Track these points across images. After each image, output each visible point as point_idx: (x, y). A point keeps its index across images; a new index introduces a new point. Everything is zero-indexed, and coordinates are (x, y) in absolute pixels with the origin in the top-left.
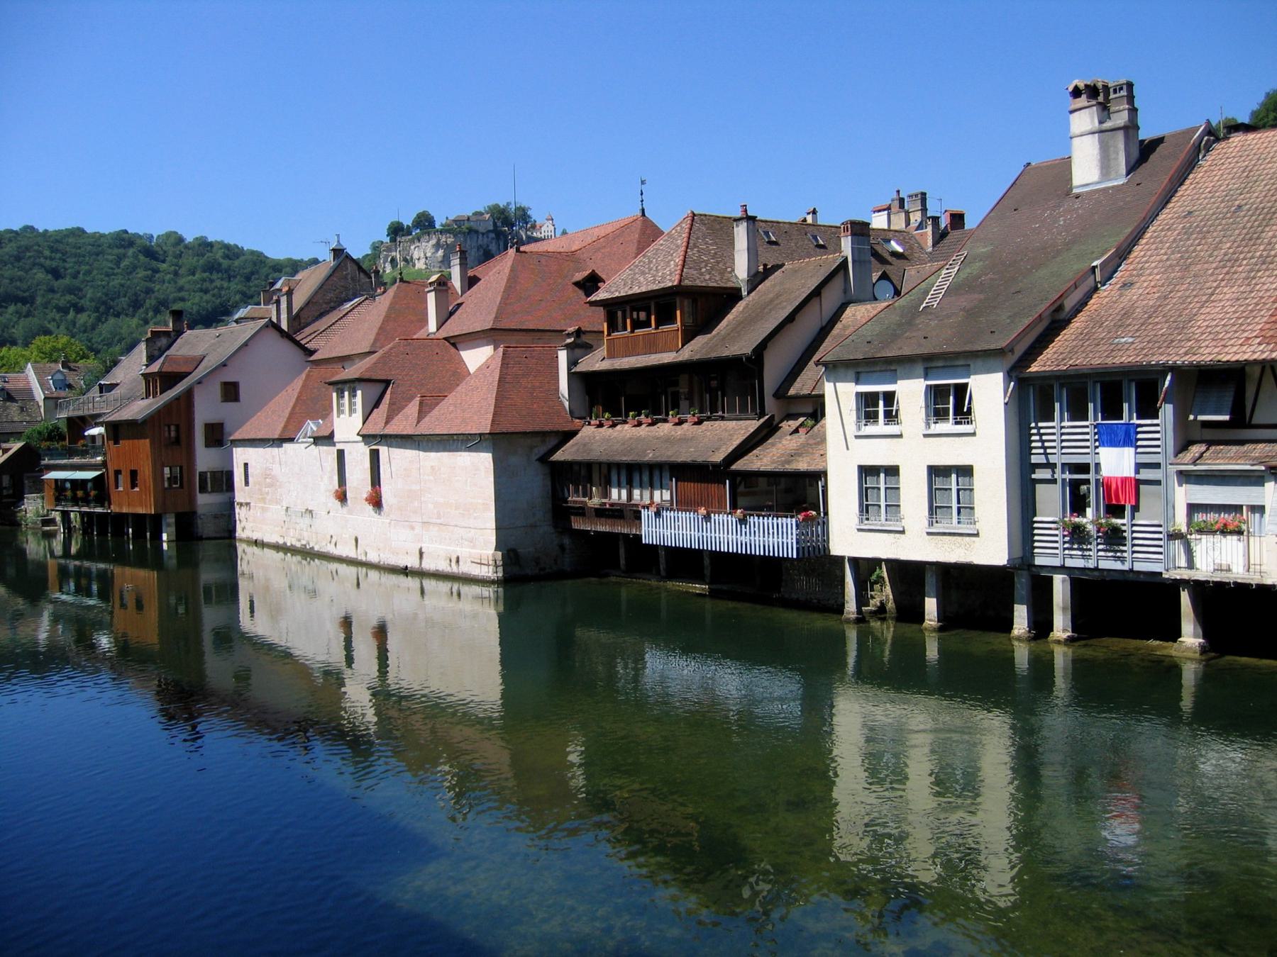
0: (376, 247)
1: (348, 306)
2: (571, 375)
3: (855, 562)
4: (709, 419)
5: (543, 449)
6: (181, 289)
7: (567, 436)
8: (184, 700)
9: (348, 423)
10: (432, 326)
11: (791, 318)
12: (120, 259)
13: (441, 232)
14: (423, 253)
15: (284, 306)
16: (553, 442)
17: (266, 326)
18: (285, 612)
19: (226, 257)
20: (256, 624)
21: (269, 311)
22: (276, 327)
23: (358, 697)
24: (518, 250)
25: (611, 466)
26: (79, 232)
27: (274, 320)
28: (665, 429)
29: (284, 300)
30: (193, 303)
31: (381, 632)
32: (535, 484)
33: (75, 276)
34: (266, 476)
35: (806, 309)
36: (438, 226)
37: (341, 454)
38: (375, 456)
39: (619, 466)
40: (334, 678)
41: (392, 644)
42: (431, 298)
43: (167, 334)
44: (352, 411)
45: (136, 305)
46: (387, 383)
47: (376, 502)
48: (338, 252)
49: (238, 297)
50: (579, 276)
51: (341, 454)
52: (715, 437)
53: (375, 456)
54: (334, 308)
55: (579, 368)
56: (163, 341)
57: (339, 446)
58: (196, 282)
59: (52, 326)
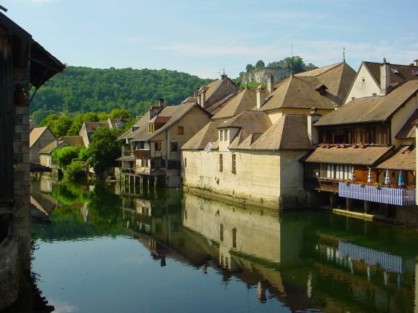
0: (241, 74)
1: (227, 98)
2: (313, 127)
3: (397, 187)
4: (368, 146)
5: (300, 156)
6: (166, 90)
7: (311, 151)
8: (162, 250)
9: (224, 144)
10: (258, 106)
11: (403, 105)
12: (145, 79)
13: (267, 68)
14: (258, 77)
15: (202, 97)
16: (304, 154)
17: (195, 106)
18: (201, 220)
19: (185, 78)
20: (188, 223)
21: (197, 99)
22: (199, 106)
23: (224, 252)
24: (293, 76)
25: (327, 164)
26: (130, 69)
27: (199, 103)
28: (351, 149)
29: (202, 95)
30: (172, 95)
31: (234, 231)
32: (296, 170)
33: (128, 85)
34: (193, 164)
35: (410, 102)
36: (266, 66)
37: (221, 155)
38: (234, 156)
39: (330, 164)
40: (216, 244)
41: (238, 234)
42: (258, 95)
43: (158, 108)
44: (226, 139)
45: (150, 96)
46: (240, 128)
47: (234, 172)
48: (224, 76)
49: (188, 94)
50: (318, 87)
51: (221, 155)
52: (371, 154)
53: (234, 156)
54: (221, 99)
55: (317, 124)
56: (156, 111)
57: (221, 153)
58: (172, 88)
59: (120, 104)
